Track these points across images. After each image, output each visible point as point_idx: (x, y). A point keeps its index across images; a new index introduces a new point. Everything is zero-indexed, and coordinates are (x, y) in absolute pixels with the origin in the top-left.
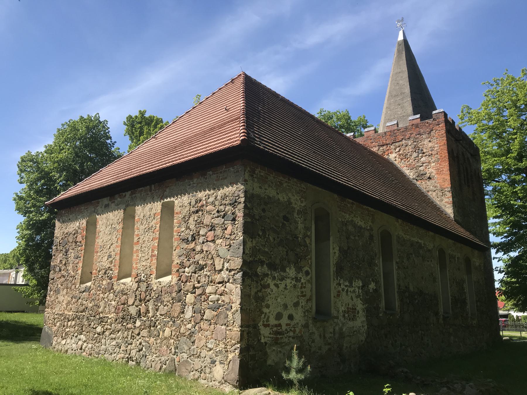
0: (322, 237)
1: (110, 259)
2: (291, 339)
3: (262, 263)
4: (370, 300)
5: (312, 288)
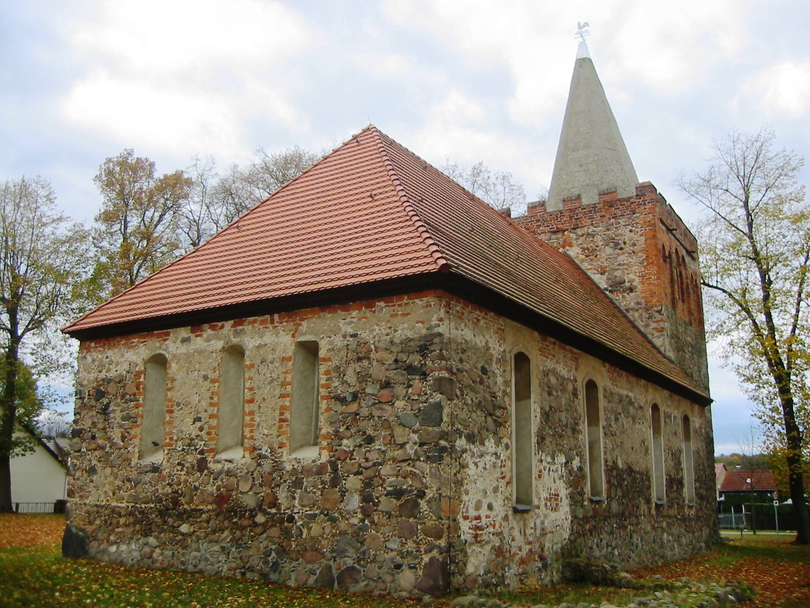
0: (523, 393)
1: (198, 424)
2: (491, 536)
3: (460, 434)
4: (575, 480)
5: (512, 467)
